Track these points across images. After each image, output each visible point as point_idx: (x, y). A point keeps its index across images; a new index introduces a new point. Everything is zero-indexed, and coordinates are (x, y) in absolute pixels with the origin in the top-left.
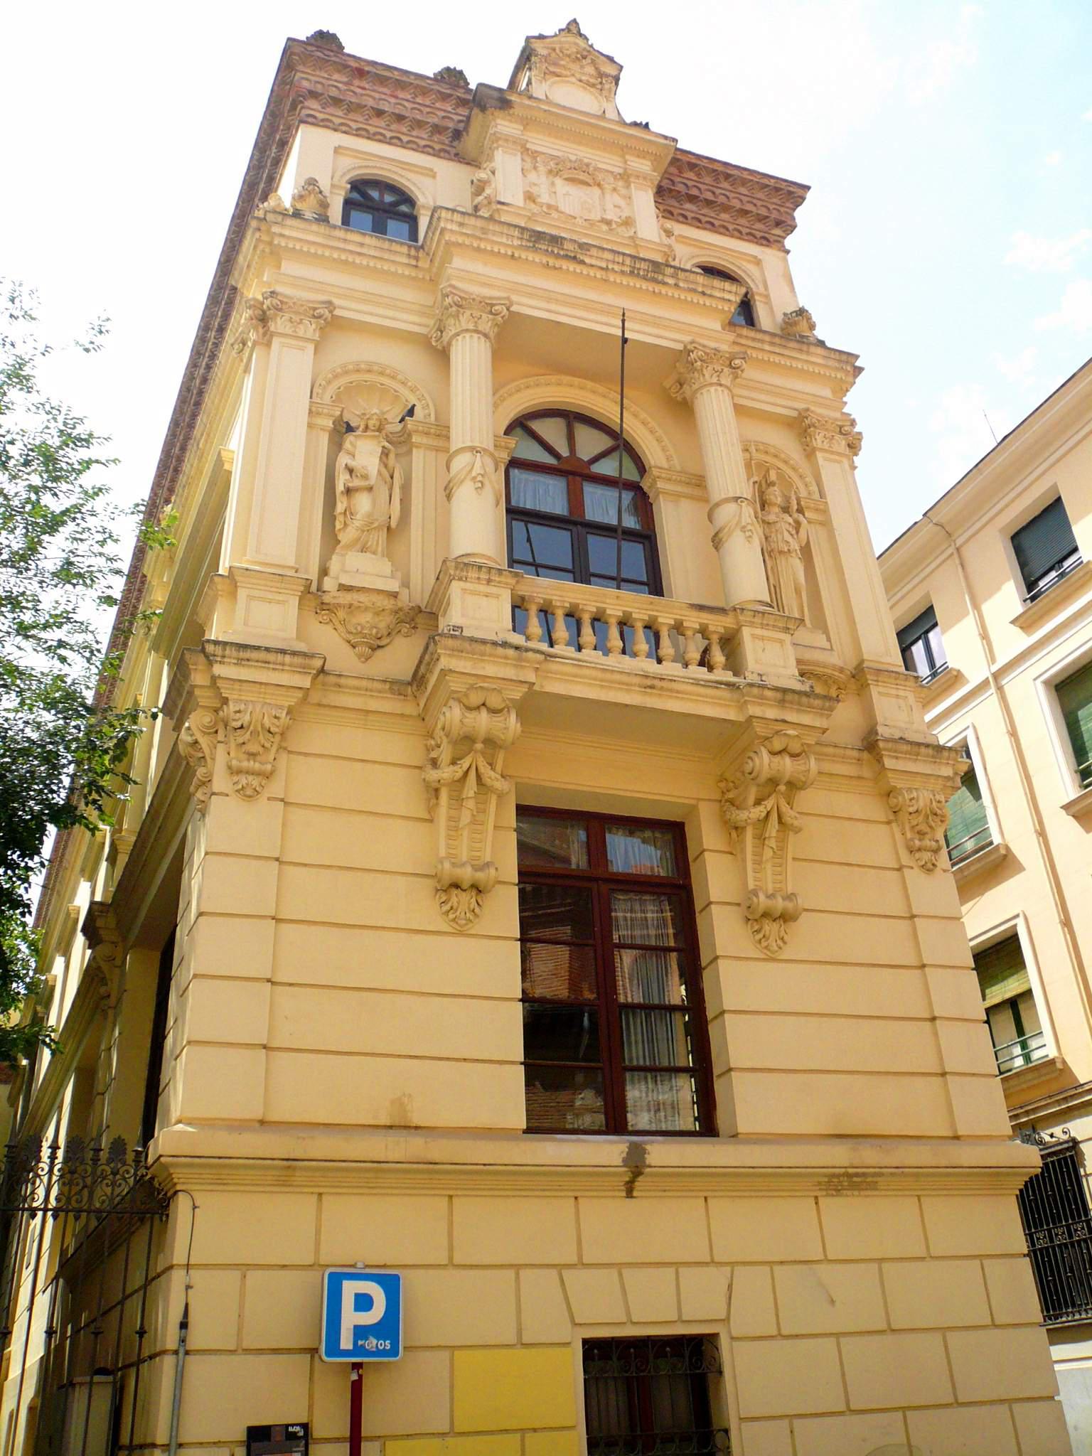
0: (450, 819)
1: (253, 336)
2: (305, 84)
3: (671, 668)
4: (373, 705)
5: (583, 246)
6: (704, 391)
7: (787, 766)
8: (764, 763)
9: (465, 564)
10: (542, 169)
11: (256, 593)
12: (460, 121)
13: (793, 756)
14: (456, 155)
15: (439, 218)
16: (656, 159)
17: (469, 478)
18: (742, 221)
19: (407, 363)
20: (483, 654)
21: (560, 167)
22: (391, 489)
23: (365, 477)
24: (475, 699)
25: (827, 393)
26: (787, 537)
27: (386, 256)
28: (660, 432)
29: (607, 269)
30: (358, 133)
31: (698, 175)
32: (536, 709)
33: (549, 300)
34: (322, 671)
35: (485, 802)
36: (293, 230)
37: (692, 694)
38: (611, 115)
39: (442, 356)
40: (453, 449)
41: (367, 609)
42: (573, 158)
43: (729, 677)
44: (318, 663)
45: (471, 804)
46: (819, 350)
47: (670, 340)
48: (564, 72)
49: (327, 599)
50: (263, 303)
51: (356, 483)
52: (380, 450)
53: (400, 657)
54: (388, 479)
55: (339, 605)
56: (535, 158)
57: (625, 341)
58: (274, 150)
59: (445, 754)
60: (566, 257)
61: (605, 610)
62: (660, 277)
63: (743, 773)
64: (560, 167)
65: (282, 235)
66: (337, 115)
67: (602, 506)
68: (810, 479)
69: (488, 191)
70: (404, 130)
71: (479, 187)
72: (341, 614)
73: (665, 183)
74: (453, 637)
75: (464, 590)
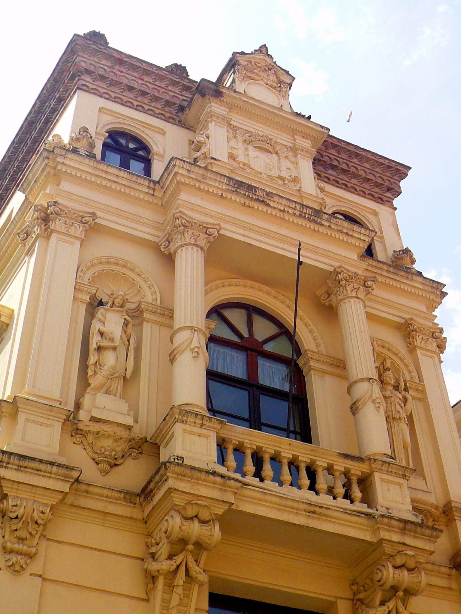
0: (163, 600)
1: (37, 230)
2: (83, 64)
3: (325, 499)
4: (111, 509)
5: (268, 194)
6: (347, 301)
7: (405, 578)
8: (389, 575)
9: (187, 412)
10: (240, 139)
11: (32, 418)
13: (410, 570)
15: (174, 166)
16: (314, 140)
18: (366, 185)
19: (143, 261)
20: (198, 479)
21: (252, 138)
22: (128, 349)
23: (112, 340)
24: (191, 512)
25: (423, 308)
26: (398, 408)
27: (133, 186)
28: (312, 327)
29: (284, 211)
30: (116, 100)
31: (339, 152)
32: (234, 523)
33: (245, 228)
34: (77, 480)
35: (190, 590)
36: (72, 161)
37: (341, 520)
38: (286, 108)
39: (169, 260)
40: (176, 327)
42: (261, 134)
43: (364, 508)
44: (75, 474)
45: (179, 590)
46: (419, 279)
47: (325, 264)
49: (81, 426)
50: (48, 209)
51: (105, 343)
53: (132, 474)
57: (300, 263)
58: (53, 103)
59: (164, 550)
61: (280, 452)
62: (319, 221)
63: (372, 580)
64: (252, 138)
65: (63, 164)
66: (102, 86)
67: (271, 375)
68: (412, 367)
69: (204, 150)
70: (146, 102)
72: (90, 438)
74: (178, 464)
75: (184, 431)
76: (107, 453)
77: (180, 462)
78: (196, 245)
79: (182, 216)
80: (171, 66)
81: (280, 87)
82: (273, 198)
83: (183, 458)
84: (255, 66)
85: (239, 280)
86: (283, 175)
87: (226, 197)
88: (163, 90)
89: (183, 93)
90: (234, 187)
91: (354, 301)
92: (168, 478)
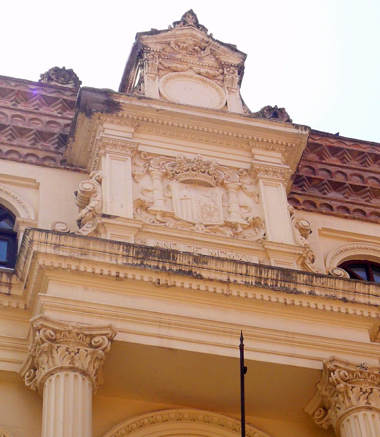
5: (199, 259)
6: (351, 417)
10: (157, 173)
12: (67, 125)
14: (63, 162)
15: (31, 242)
16: (287, 149)
21: (175, 169)
29: (228, 282)
31: (342, 160)
33: (160, 324)
39: (35, 396)
47: (307, 359)
48: (179, 66)
56: (148, 161)
60: (180, 273)
62: (292, 286)
64: (175, 169)
69: (93, 204)
71: (84, 199)
73: (304, 172)
78: (73, 369)
79: (45, 324)
80: (48, 73)
81: (223, 74)
82: (206, 263)
84: (177, 49)
85: (169, 411)
86: (235, 218)
87: (126, 277)
88: (32, 116)
89: (65, 114)
90: (138, 259)
91: (365, 415)
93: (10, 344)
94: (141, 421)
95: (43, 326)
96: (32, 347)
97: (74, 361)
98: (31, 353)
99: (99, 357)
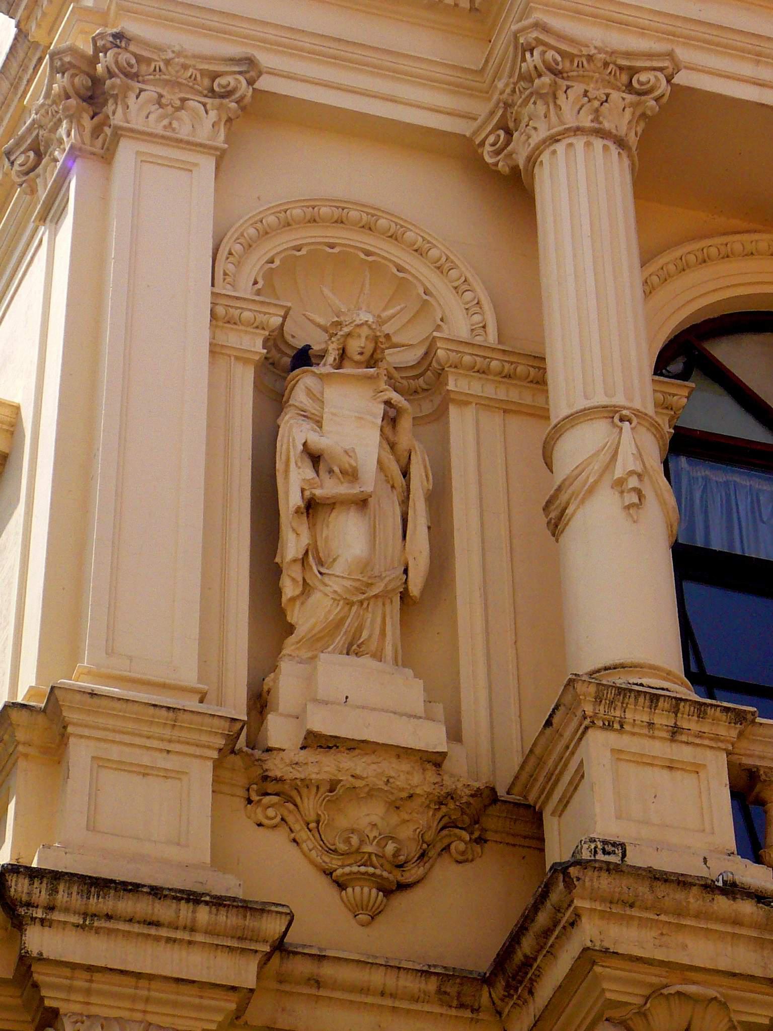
9: (622, 691)
11: (115, 752)
17: (607, 481)
19: (429, 204)
22: (405, 501)
23: (351, 475)
34: (280, 947)
39: (513, 191)
41: (372, 793)
44: (273, 927)
49: (276, 767)
50: (94, 60)
51: (329, 488)
52: (380, 409)
54: (399, 479)
55: (307, 783)
72: (310, 805)
74: (609, 868)
76: (368, 849)
77: (614, 859)
79: (542, 37)
83: (623, 845)
85: (756, 236)
92: (578, 916)
93: (448, 77)
94: (705, 250)
95: (539, 42)
96: (507, 85)
97: (601, 119)
98: (505, 96)
99: (649, 113)
